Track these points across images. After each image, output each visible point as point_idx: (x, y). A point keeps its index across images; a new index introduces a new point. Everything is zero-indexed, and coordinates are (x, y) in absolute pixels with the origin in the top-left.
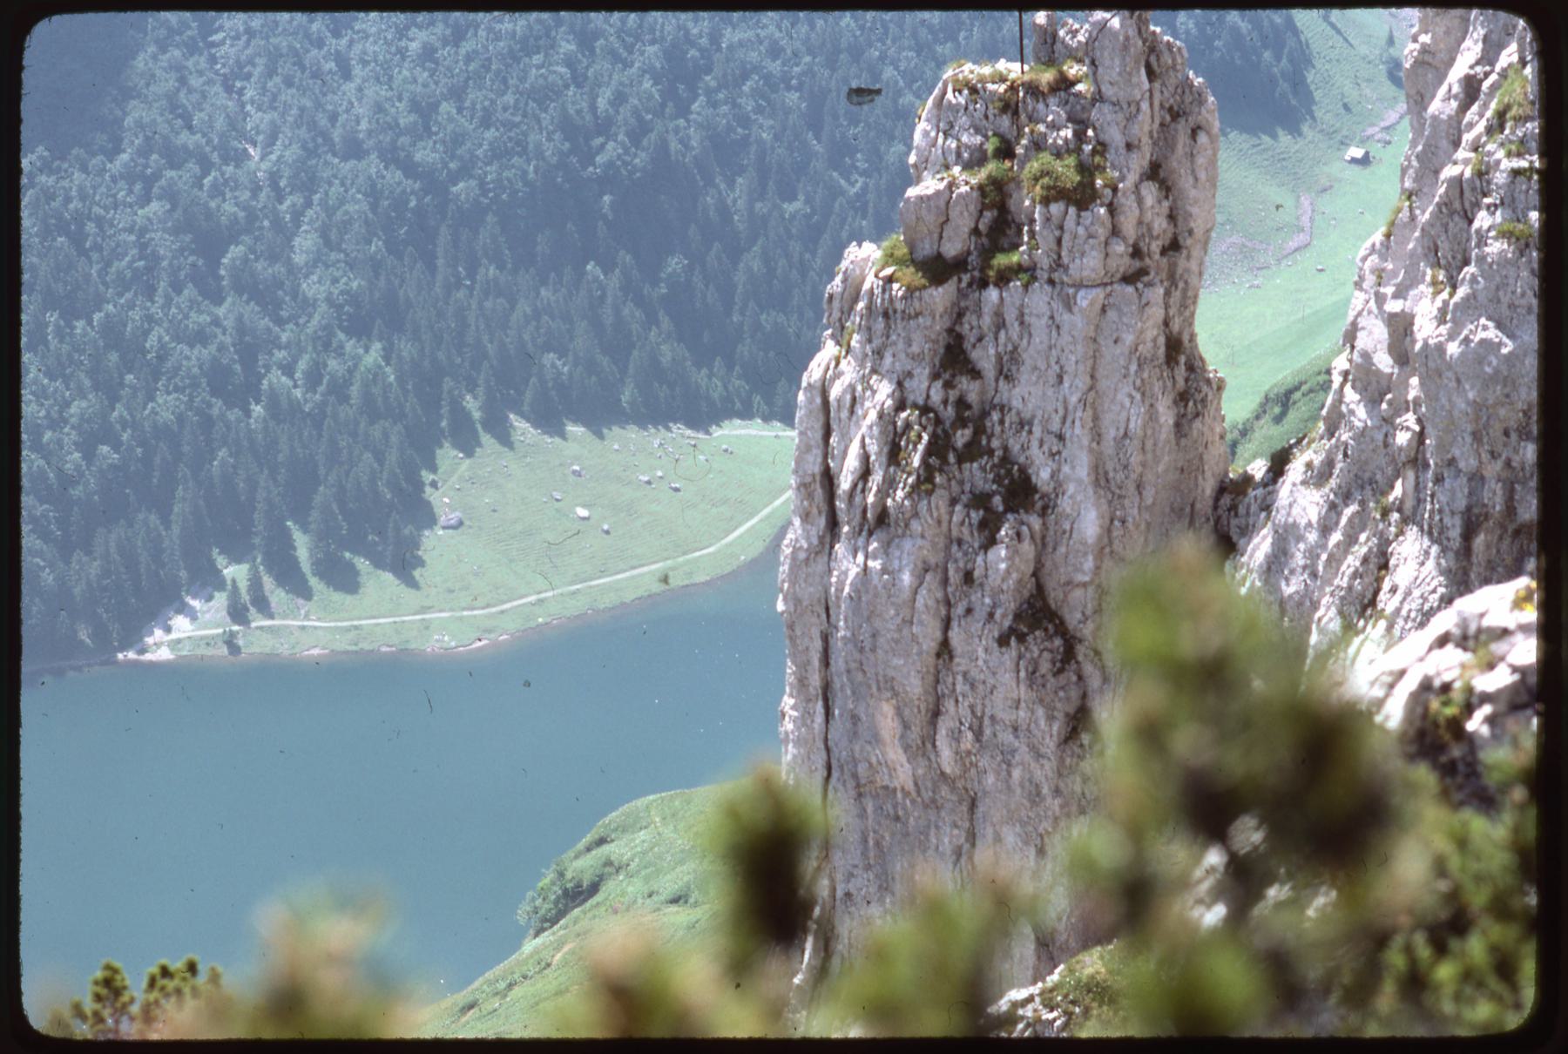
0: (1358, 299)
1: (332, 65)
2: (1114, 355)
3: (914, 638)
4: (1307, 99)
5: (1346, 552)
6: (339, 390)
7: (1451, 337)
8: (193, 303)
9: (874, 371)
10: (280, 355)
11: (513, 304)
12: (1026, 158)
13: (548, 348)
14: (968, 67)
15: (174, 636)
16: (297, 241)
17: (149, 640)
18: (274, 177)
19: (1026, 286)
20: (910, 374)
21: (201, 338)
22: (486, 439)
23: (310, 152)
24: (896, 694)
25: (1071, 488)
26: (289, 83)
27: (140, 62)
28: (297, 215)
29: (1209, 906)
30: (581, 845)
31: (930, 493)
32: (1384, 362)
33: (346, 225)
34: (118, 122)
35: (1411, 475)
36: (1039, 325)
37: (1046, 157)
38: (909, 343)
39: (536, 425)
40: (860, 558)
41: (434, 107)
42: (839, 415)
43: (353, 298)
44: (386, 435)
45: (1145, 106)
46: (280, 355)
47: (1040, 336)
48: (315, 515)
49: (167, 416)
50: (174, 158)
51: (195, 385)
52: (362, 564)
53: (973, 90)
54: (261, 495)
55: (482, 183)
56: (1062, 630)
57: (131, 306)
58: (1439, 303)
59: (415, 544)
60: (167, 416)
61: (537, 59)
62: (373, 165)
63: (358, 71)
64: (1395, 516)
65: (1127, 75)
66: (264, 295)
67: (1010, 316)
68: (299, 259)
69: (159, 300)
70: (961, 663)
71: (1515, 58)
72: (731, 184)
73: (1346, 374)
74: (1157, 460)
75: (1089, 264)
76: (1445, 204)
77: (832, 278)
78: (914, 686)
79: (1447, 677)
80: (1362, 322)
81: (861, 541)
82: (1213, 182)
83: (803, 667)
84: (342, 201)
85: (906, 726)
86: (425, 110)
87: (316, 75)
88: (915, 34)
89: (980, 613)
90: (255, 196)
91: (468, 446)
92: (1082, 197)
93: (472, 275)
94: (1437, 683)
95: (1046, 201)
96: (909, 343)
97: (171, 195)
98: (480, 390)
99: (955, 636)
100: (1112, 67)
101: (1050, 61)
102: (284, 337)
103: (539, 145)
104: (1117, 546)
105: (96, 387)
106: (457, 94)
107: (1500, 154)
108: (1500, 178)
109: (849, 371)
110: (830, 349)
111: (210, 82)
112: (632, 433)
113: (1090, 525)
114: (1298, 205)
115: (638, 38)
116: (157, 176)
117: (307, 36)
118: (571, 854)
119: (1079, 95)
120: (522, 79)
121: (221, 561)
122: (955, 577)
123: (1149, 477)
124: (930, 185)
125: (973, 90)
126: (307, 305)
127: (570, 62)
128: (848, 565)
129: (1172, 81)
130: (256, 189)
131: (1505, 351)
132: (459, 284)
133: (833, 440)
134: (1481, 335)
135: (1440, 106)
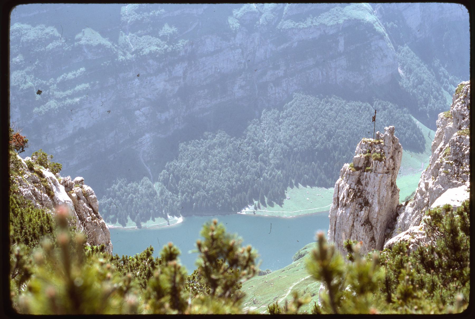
0: (421, 180)
1: (278, 129)
2: (383, 184)
3: (348, 223)
4: (424, 148)
5: (415, 218)
6: (274, 177)
7: (434, 187)
8: (254, 162)
9: (346, 183)
10: (266, 171)
11: (301, 166)
12: (373, 153)
13: (305, 174)
14: (366, 139)
15: (246, 211)
16: (270, 155)
17: (242, 211)
18: (268, 145)
19: (371, 172)
20: (352, 184)
21: (254, 167)
22: (295, 186)
23: (274, 142)
24: (345, 232)
25: (374, 204)
26: (271, 131)
27: (250, 126)
28: (271, 151)
29: (378, 270)
30: (302, 249)
31: (353, 202)
32: (424, 190)
33: (277, 153)
34: (246, 135)
35: (426, 207)
36: (372, 178)
37: (376, 153)
38: (352, 179)
39: (302, 185)
40: (342, 210)
41: (293, 137)
42: (341, 189)
43: (278, 164)
44: (280, 185)
45: (392, 147)
46: (266, 171)
47: (372, 180)
48: (268, 195)
49: (248, 178)
50: (254, 140)
51: (253, 174)
52: (275, 203)
53: (366, 142)
54: (261, 191)
55: (298, 149)
56: (371, 225)
57: (245, 161)
58: (433, 181)
59: (283, 201)
60: (248, 178)
61: (309, 131)
62: (283, 144)
63: (282, 130)
64: (423, 213)
65: (389, 142)
66: (265, 162)
67: (368, 177)
68: (270, 157)
69: (249, 161)
70: (355, 228)
71: (448, 146)
72: (335, 152)
73: (418, 191)
74: (388, 201)
75: (380, 170)
76: (435, 167)
77: (342, 168)
78: (348, 231)
79: (407, 239)
80: (421, 183)
81: (342, 208)
82: (401, 159)
83: (332, 226)
84: (277, 149)
85: (346, 237)
86: (291, 137)
87: (276, 130)
88: (366, 133)
89: (359, 221)
90: (265, 147)
91: (292, 187)
92: (380, 160)
93: (295, 162)
94: (405, 240)
95: (375, 160)
96: (352, 179)
97: (252, 146)
98: (295, 179)
99: (355, 224)
100: (387, 141)
101: (378, 139)
102: (267, 168)
103: (307, 144)
104: (381, 213)
105: (239, 173)
106: (296, 135)
107: (445, 160)
108: (444, 164)
109: (343, 182)
110: (340, 179)
111: (260, 130)
112: (317, 188)
113: (377, 209)
114: (421, 164)
115: (324, 129)
116: (251, 143)
117: (275, 125)
118: (301, 250)
119: (382, 145)
120: (306, 134)
121: (254, 200)
122: (355, 215)
123: (386, 203)
124: (358, 156)
125: (366, 142)
126: (271, 164)
127: (313, 132)
128: (340, 211)
129: (396, 144)
130: (265, 146)
131: (443, 190)
132: (293, 163)
133: (339, 193)
134: (439, 187)
135: (436, 152)
